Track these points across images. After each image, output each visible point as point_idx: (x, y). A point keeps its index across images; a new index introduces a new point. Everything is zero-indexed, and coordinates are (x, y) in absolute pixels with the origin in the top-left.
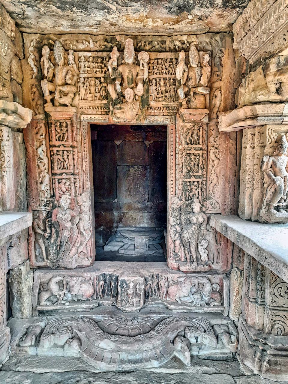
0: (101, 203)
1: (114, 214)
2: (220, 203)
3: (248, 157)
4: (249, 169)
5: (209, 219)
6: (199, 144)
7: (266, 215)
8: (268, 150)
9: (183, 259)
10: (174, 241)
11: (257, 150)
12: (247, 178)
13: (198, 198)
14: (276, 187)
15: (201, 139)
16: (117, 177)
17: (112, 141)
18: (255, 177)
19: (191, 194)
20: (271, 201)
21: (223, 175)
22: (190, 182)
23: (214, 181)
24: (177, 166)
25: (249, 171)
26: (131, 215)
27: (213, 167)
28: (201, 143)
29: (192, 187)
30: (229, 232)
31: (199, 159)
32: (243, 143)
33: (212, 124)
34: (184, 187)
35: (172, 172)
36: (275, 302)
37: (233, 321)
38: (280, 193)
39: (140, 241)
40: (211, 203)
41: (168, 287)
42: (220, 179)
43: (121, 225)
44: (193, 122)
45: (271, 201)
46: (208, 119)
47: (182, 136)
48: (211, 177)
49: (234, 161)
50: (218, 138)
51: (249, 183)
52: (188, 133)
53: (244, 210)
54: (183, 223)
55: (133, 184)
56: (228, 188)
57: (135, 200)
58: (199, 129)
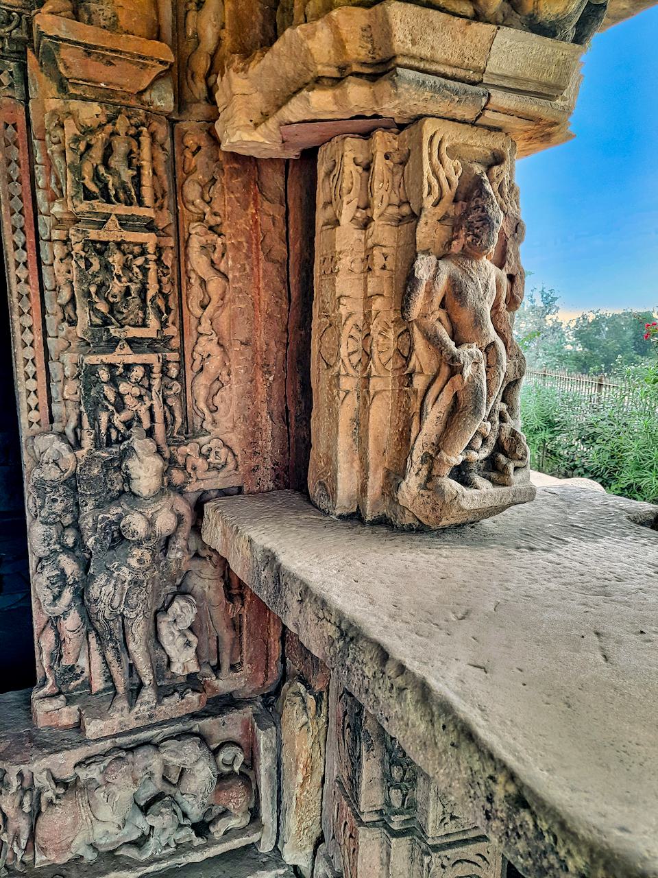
3: (344, 263)
4: (350, 315)
6: (141, 203)
7: (419, 501)
8: (428, 231)
9: (98, 684)
11: (382, 232)
12: (343, 352)
13: (150, 433)
14: (459, 386)
15: (147, 180)
18: (375, 349)
19: (118, 419)
20: (440, 444)
21: (243, 339)
22: (112, 367)
23: (213, 365)
24: (46, 294)
25: (350, 323)
27: (204, 307)
29: (123, 387)
30: (292, 600)
31: (144, 270)
32: (319, 205)
33: (190, 125)
34: (87, 390)
35: (27, 321)
36: (453, 818)
37: (295, 867)
38: (476, 411)
40: (204, 450)
41: (36, 814)
42: (232, 355)
44: (105, 97)
45: (440, 444)
46: (170, 98)
47: (57, 160)
48: (199, 348)
49: (279, 285)
50: (218, 185)
51: (351, 371)
52: (89, 147)
53: (335, 480)
58: (137, 136)
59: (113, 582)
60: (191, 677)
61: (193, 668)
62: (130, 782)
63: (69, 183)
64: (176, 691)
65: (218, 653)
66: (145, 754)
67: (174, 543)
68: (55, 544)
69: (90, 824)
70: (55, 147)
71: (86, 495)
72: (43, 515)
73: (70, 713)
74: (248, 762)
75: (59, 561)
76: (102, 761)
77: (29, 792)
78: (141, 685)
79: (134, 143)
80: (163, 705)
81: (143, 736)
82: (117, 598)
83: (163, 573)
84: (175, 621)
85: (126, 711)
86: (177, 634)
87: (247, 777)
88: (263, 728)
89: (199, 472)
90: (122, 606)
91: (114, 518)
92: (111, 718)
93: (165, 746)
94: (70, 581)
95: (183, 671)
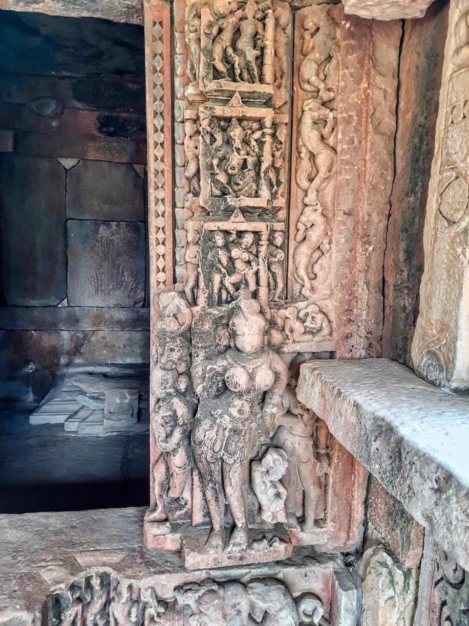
1: (60, 336)
2: (333, 317)
5: (294, 369)
6: (262, 81)
9: (198, 518)
10: (166, 456)
15: (269, 59)
16: (66, 246)
17: (52, 157)
19: (229, 281)
21: (346, 208)
22: (227, 233)
23: (315, 235)
24: (177, 169)
26: (104, 338)
27: (311, 180)
28: (268, 77)
29: (235, 252)
31: (261, 143)
35: (161, 194)
39: (118, 401)
40: (301, 315)
43: (78, 361)
47: (193, 47)
52: (220, 31)
54: (199, 389)
55: (106, 265)
56: (361, 260)
57: (112, 302)
59: (216, 428)
60: (278, 526)
61: (282, 518)
63: (202, 65)
64: (264, 537)
66: (235, 592)
67: (271, 398)
70: (192, 35)
72: (162, 361)
74: (327, 616)
75: (173, 404)
76: (197, 591)
77: (136, 604)
79: (260, 25)
80: (252, 549)
83: (259, 425)
84: (268, 471)
85: (220, 549)
86: (269, 484)
88: (346, 589)
89: (296, 335)
90: (222, 451)
91: (220, 370)
92: (207, 553)
94: (180, 422)
95: (272, 520)
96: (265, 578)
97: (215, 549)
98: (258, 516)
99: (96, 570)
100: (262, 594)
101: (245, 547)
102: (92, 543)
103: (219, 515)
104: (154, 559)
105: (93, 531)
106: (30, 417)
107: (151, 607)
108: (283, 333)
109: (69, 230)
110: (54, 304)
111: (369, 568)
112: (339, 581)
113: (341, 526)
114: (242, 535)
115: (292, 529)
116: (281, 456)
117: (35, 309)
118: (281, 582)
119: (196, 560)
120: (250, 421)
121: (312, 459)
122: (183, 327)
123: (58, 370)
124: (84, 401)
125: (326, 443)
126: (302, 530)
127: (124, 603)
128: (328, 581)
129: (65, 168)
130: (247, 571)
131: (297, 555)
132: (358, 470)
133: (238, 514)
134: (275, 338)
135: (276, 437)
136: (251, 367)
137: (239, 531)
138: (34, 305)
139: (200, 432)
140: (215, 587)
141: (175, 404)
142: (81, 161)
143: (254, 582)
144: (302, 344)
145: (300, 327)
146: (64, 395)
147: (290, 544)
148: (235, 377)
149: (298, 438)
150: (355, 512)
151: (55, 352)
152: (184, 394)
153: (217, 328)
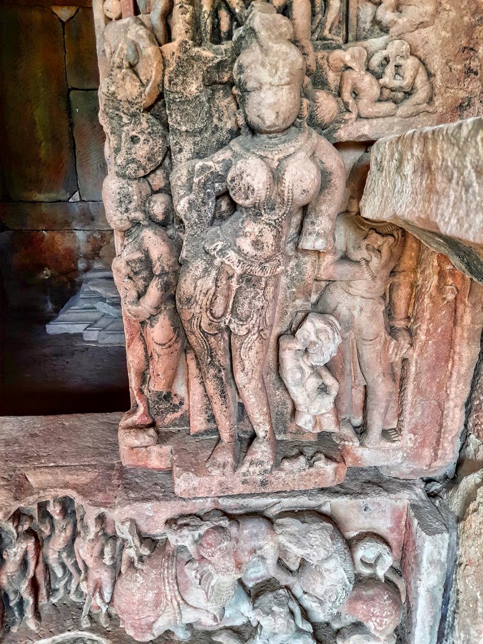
0: (35, 202)
1: (75, 237)
2: (436, 63)
9: (198, 423)
16: (72, 125)
40: (376, 61)
59: (214, 273)
60: (324, 437)
61: (329, 425)
62: (230, 564)
64: (301, 453)
65: (365, 409)
66: (255, 531)
67: (313, 223)
68: (136, 210)
69: (176, 607)
71: (181, 132)
72: (119, 162)
73: (160, 455)
74: (397, 565)
75: (142, 239)
76: (197, 527)
77: (111, 541)
78: (254, 436)
80: (282, 470)
81: (256, 503)
82: (220, 301)
83: (292, 279)
84: (306, 350)
85: (229, 469)
86: (308, 371)
87: (395, 587)
88: (432, 532)
89: (364, 101)
90: (228, 316)
91: (218, 168)
92: (208, 473)
93: (282, 525)
94: (157, 270)
95: (314, 427)
96: (302, 511)
97: (221, 469)
98: (291, 421)
99: (53, 493)
100: (298, 535)
101: (269, 467)
102: (53, 456)
103: (228, 417)
104: (138, 481)
105: (60, 441)
106: (47, 326)
107: (131, 547)
108: (339, 99)
109: (73, 104)
110: (64, 198)
111: (476, 503)
112: (419, 519)
113: (424, 440)
114: (265, 449)
115: (346, 443)
116: (331, 324)
117: (43, 204)
118: (328, 518)
119: (191, 485)
120: (275, 263)
121: (383, 334)
122: (148, 89)
123: (76, 277)
124: (104, 308)
125: (407, 312)
126: (362, 445)
127: (93, 540)
128: (400, 517)
129: (61, 21)
130: (275, 500)
131: (352, 480)
132: (460, 353)
133: (257, 416)
134: (323, 107)
135: (321, 301)
136: (277, 157)
137: (261, 443)
138: (41, 200)
139: (187, 282)
140: (225, 523)
141: (146, 240)
142: (80, 10)
143: (284, 517)
144: (375, 121)
145: (372, 85)
146: (82, 302)
147: (343, 464)
148: (244, 175)
149: (359, 300)
150: (448, 419)
151: (71, 255)
152: (164, 224)
153: (213, 94)
